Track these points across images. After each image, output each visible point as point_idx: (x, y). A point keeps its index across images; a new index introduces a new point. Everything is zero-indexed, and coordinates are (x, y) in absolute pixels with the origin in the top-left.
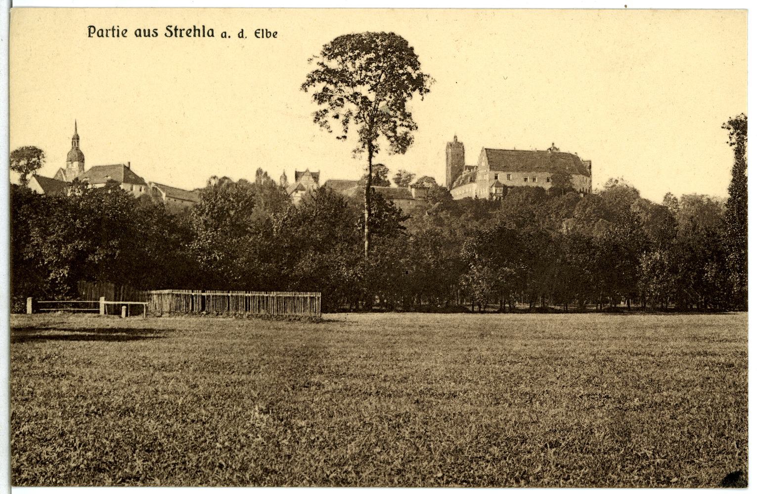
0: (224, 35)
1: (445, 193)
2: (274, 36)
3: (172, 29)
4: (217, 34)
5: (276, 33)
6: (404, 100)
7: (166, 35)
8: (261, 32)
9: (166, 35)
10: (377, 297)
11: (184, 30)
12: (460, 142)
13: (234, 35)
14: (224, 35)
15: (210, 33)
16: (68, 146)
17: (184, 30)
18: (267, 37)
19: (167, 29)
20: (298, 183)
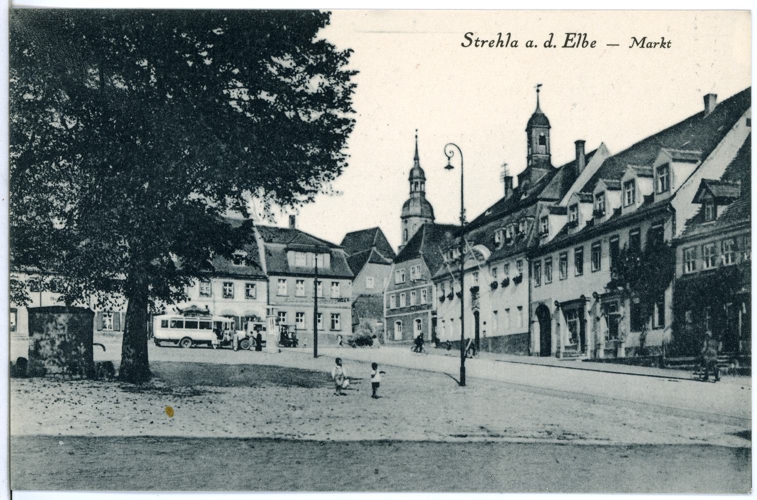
0: (530, 45)
1: (252, 226)
2: (592, 47)
3: (474, 38)
4: (522, 44)
5: (595, 42)
6: (521, 177)
7: (463, 45)
8: (578, 37)
9: (463, 45)
10: (208, 62)
11: (487, 41)
12: (446, 341)
13: (522, 44)
14: (530, 45)
15: (514, 44)
16: (404, 191)
17: (487, 41)
18: (583, 46)
19: (466, 37)
20: (355, 333)
